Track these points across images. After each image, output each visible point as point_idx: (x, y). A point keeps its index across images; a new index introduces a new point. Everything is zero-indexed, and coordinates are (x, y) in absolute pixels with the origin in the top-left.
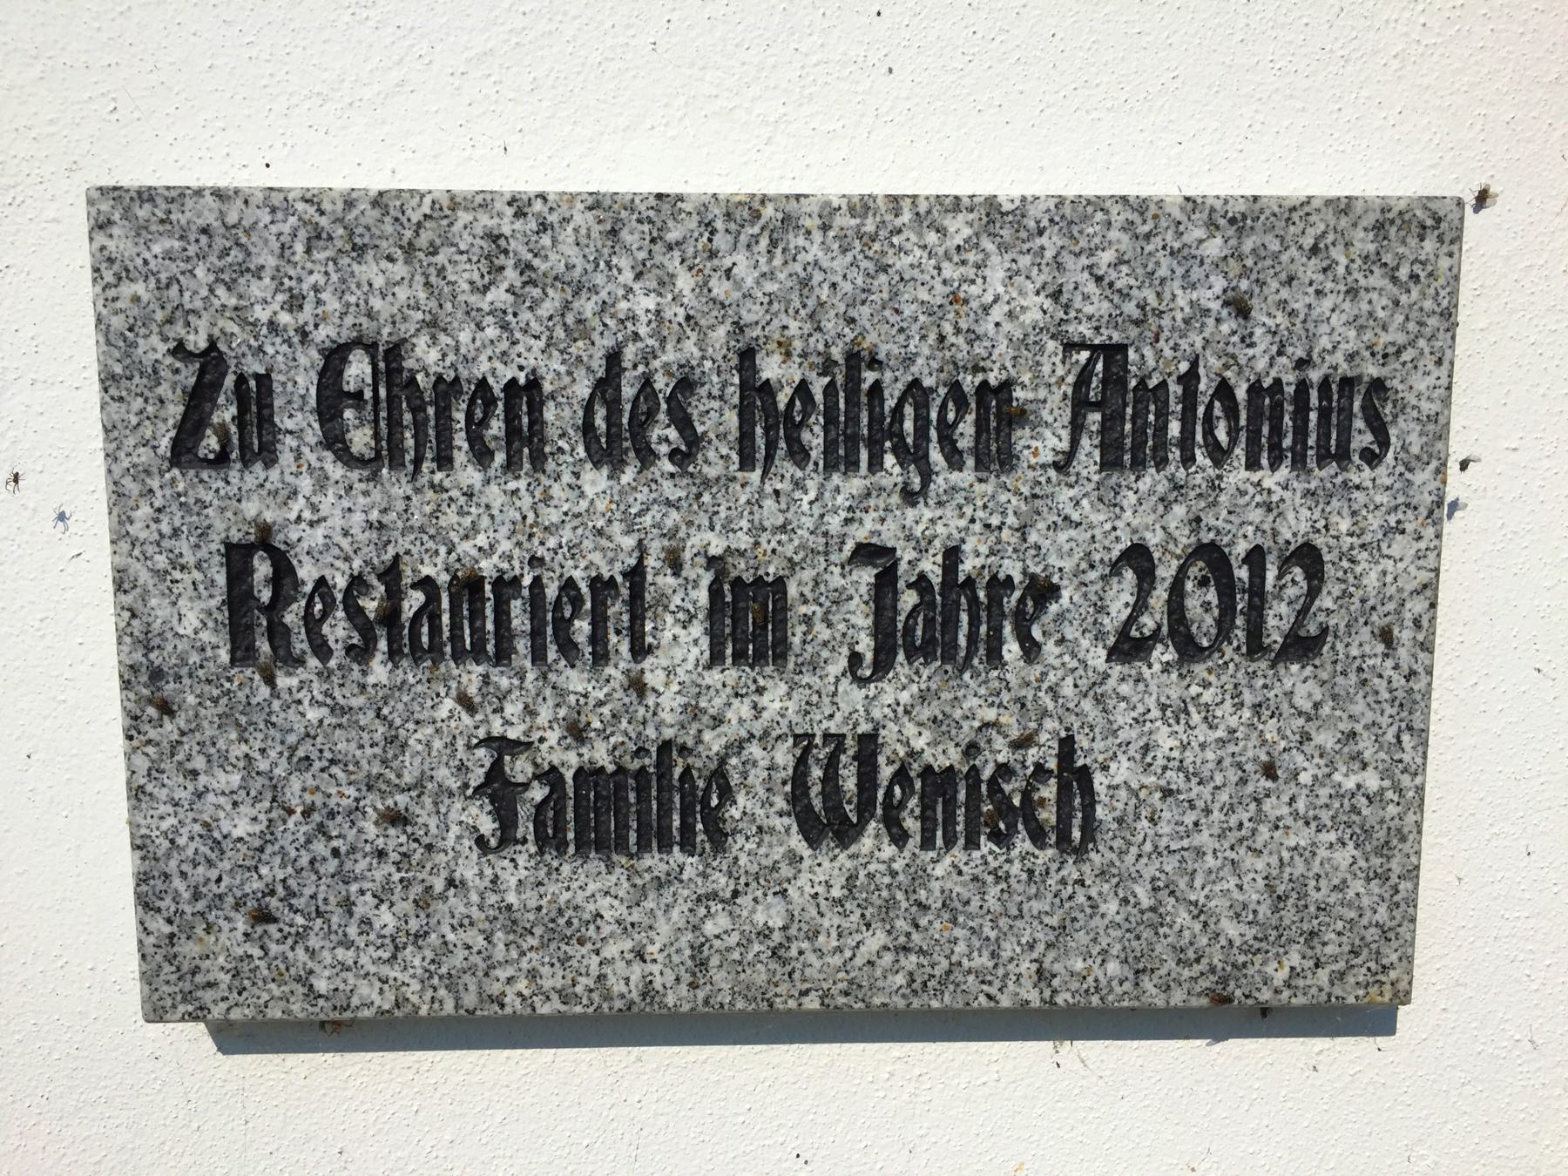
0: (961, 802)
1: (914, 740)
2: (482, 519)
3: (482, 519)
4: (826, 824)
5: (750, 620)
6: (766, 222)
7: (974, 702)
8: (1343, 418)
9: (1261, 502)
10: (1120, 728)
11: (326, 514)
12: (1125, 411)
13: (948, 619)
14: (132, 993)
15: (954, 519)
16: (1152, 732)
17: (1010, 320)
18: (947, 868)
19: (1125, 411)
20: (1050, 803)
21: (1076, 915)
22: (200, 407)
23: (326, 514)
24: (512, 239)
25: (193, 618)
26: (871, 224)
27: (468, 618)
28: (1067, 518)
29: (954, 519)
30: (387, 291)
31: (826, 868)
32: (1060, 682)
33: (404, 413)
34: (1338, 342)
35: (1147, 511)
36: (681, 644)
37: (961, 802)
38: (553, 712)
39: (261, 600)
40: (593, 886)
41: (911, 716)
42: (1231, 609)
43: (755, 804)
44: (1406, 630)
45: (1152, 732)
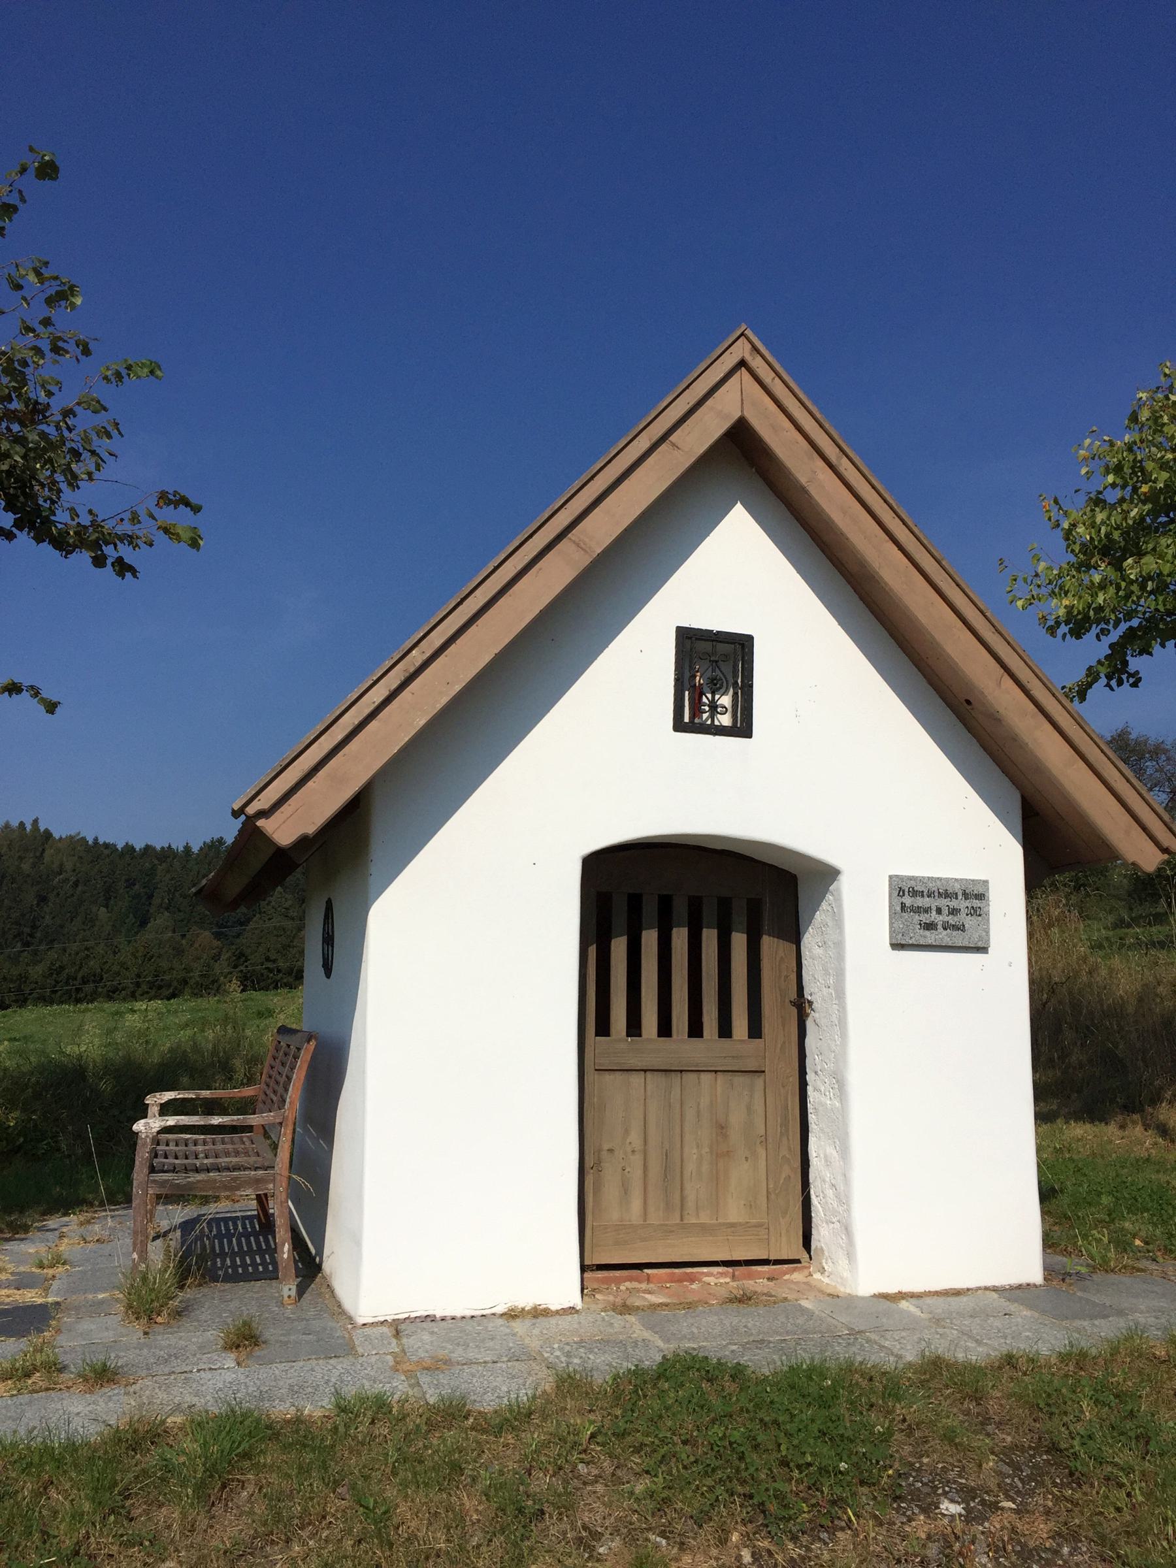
0: (956, 928)
1: (951, 922)
2: (920, 902)
3: (920, 902)
4: (945, 929)
5: (939, 911)
6: (940, 879)
7: (956, 919)
8: (981, 897)
9: (976, 903)
10: (1155, 977)
11: (908, 901)
12: (966, 896)
13: (954, 912)
14: (685, 624)
15: (954, 903)
16: (969, 922)
17: (957, 888)
18: (955, 933)
19: (966, 896)
20: (960, 928)
21: (958, 939)
22: (901, 892)
23: (908, 901)
24: (921, 880)
25: (899, 908)
26: (947, 880)
27: (918, 910)
28: (962, 904)
29: (954, 903)
30: (913, 883)
31: (945, 932)
32: (962, 918)
33: (914, 893)
34: (981, 891)
35: (968, 903)
36: (934, 913)
37: (956, 928)
38: (925, 918)
39: (903, 906)
40: (927, 933)
41: (952, 920)
42: (975, 912)
43: (939, 927)
44: (987, 914)
45: (969, 922)
